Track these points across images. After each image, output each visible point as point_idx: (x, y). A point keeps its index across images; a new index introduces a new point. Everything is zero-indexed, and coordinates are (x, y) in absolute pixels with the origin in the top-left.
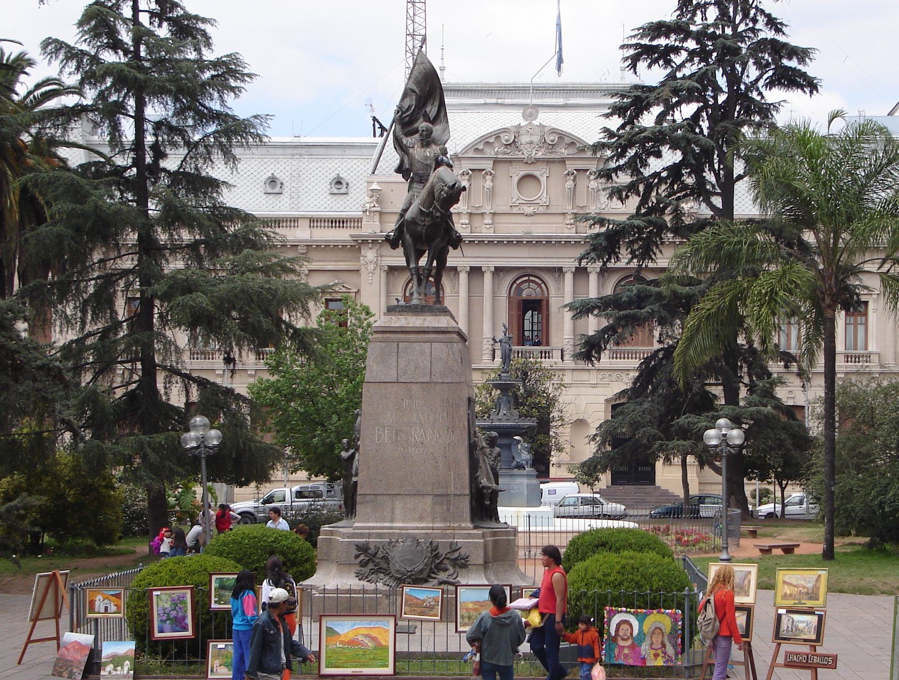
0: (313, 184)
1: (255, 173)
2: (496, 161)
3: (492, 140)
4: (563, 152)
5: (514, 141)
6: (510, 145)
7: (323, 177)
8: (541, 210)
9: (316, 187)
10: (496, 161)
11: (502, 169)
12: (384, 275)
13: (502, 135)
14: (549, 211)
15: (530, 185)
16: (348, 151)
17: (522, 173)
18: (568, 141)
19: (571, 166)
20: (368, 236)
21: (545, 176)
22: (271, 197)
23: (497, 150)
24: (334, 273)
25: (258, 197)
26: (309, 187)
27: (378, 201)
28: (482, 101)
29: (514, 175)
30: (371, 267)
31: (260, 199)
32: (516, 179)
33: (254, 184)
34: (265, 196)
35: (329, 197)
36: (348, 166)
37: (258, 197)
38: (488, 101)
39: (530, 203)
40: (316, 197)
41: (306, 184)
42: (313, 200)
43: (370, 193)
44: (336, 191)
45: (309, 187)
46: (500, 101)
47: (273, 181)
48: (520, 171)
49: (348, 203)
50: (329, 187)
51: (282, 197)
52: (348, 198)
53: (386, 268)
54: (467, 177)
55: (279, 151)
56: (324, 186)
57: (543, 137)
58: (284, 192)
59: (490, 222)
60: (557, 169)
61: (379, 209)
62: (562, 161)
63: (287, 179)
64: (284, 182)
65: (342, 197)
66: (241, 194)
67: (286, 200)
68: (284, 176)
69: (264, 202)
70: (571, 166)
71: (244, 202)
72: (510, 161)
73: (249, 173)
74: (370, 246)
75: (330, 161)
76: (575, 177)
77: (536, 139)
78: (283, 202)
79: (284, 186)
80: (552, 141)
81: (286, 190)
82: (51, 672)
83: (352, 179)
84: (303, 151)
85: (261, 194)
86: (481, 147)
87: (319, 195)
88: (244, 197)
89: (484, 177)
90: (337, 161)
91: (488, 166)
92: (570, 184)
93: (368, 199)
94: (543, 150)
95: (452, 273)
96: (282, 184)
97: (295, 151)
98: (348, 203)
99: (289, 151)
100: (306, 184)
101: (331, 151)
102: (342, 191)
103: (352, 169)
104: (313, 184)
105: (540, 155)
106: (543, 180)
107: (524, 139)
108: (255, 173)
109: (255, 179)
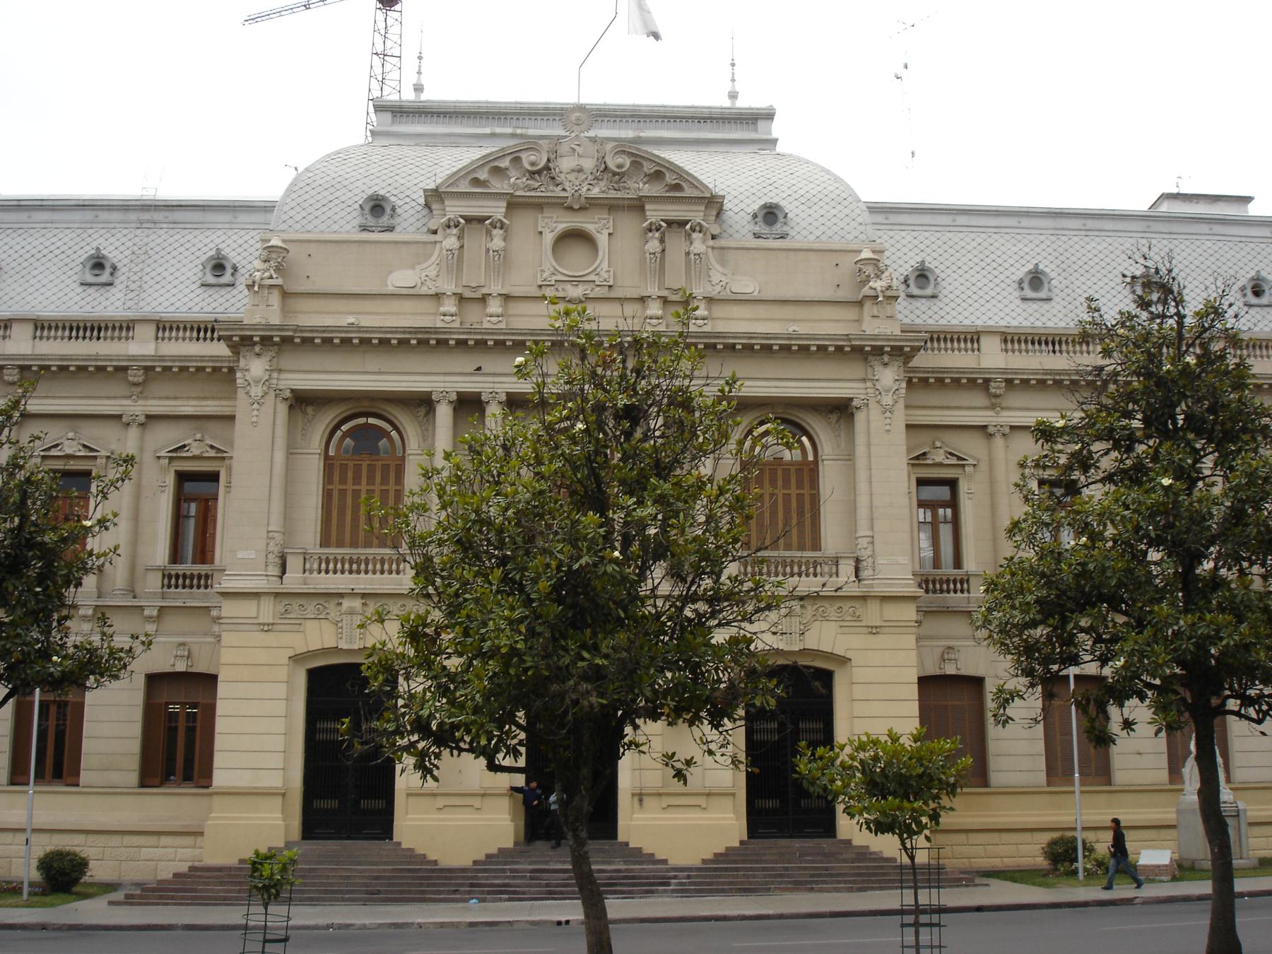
0: (172, 270)
1: (70, 252)
2: (514, 205)
3: (505, 163)
4: (639, 187)
5: (547, 168)
6: (539, 172)
7: (192, 257)
8: (599, 292)
9: (177, 274)
10: (514, 205)
11: (523, 223)
12: (283, 409)
13: (524, 156)
14: (613, 295)
15: (577, 253)
16: (243, 217)
17: (562, 227)
18: (648, 168)
19: (655, 214)
20: (254, 327)
21: (606, 232)
22: (91, 290)
23: (515, 183)
24: (194, 424)
25: (67, 290)
26: (166, 274)
27: (277, 269)
28: (488, 131)
29: (546, 232)
30: (257, 391)
31: (72, 295)
32: (549, 238)
33: (66, 269)
34: (80, 289)
35: (200, 291)
36: (240, 241)
37: (67, 290)
38: (498, 130)
39: (576, 281)
40: (175, 291)
41: (160, 270)
42: (167, 295)
43: (265, 253)
44: (212, 280)
45: (166, 274)
46: (519, 131)
47: (98, 264)
48: (564, 222)
49: (233, 301)
50: (200, 275)
51: (113, 290)
52: (235, 292)
53: (288, 394)
54: (455, 231)
55: (116, 216)
56: (192, 269)
57: (602, 160)
58: (117, 282)
59: (500, 310)
60: (629, 225)
61: (279, 281)
62: (638, 206)
63: (126, 261)
64: (119, 265)
65: (223, 291)
66: (38, 285)
67: (119, 295)
68: (120, 257)
69: (78, 298)
70: (655, 214)
71: (41, 298)
72: (539, 206)
73: (57, 252)
74: (257, 349)
75: (208, 233)
76: (663, 234)
77: (589, 164)
78: (113, 299)
79: (118, 274)
80: (620, 166)
81: (120, 279)
82: (992, 384)
83: (244, 262)
84: (158, 216)
85: (76, 285)
86: (483, 175)
87: (181, 287)
88: (42, 290)
89: (489, 233)
90: (219, 233)
91: (497, 210)
92: (654, 245)
93: (258, 264)
94: (602, 184)
95: (422, 411)
96: (114, 268)
97: (146, 216)
98: (233, 301)
99: (133, 216)
100: (160, 270)
101: (210, 217)
102: (223, 280)
103: (245, 246)
104: (172, 270)
105: (595, 192)
106: (602, 240)
107: (566, 164)
108: (70, 252)
109: (67, 260)
